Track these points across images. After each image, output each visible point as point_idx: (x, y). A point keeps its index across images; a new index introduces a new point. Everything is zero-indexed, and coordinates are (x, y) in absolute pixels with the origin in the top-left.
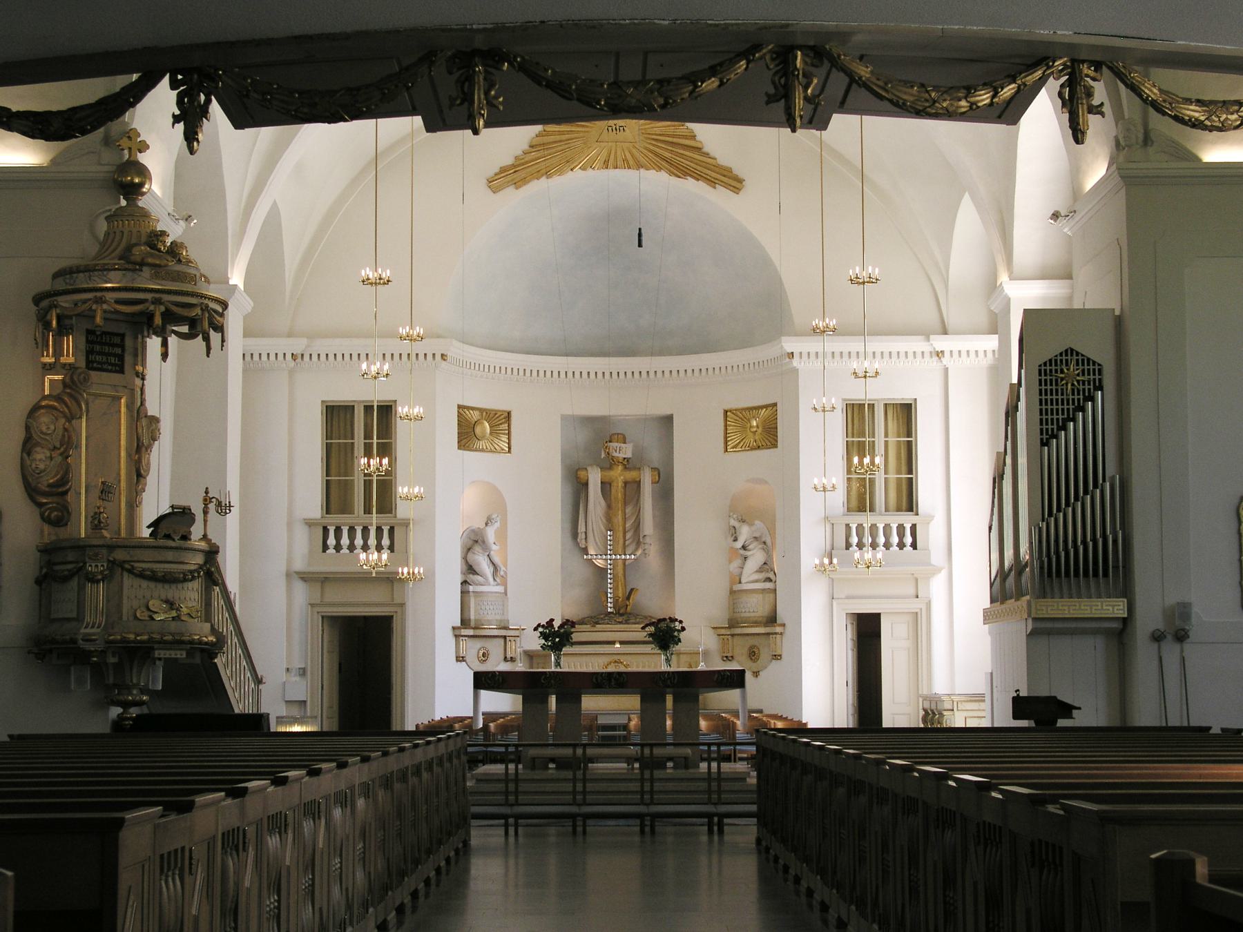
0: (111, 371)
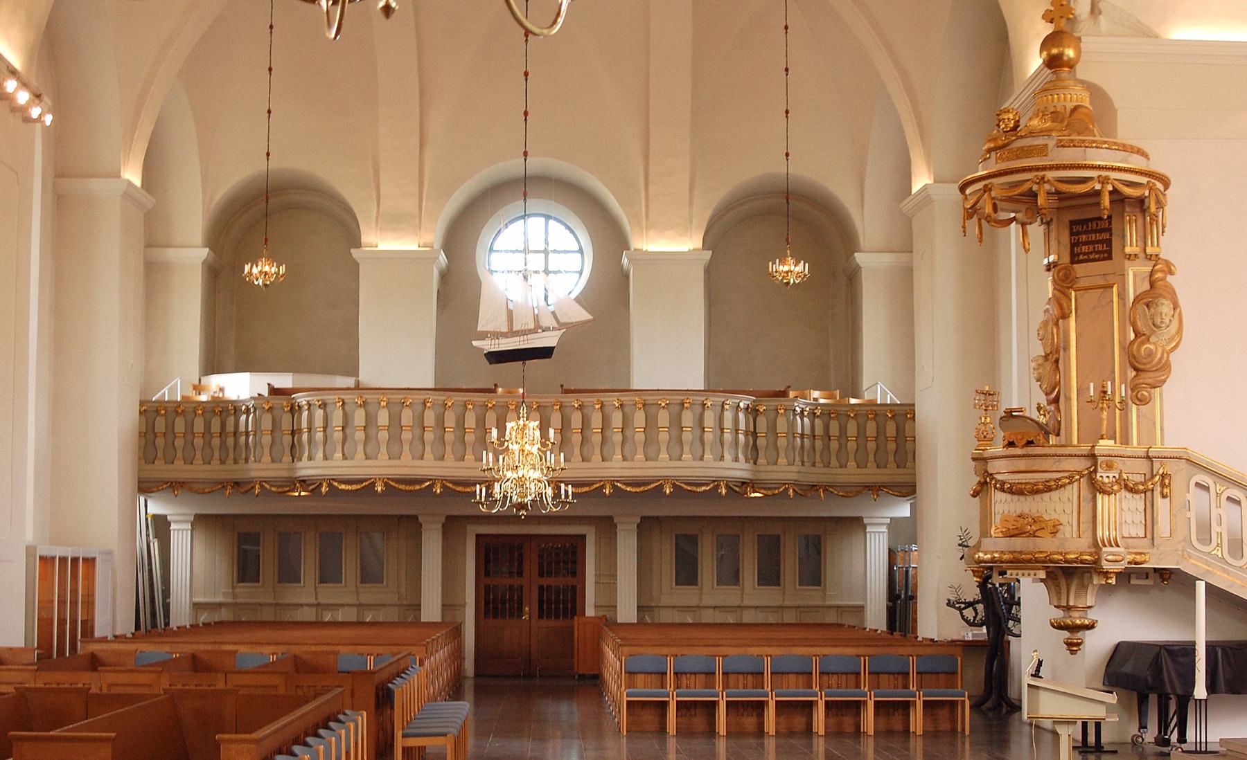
0: (1099, 260)
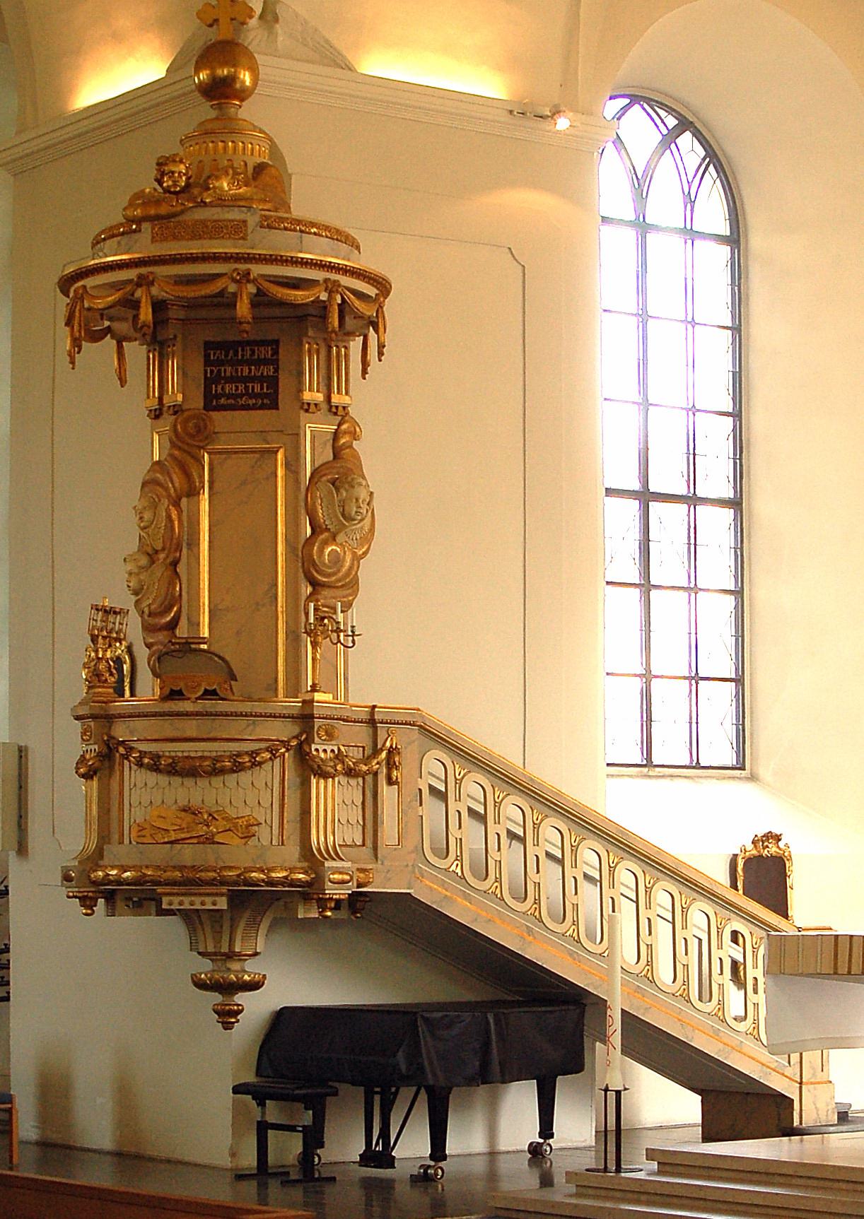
0: (253, 408)
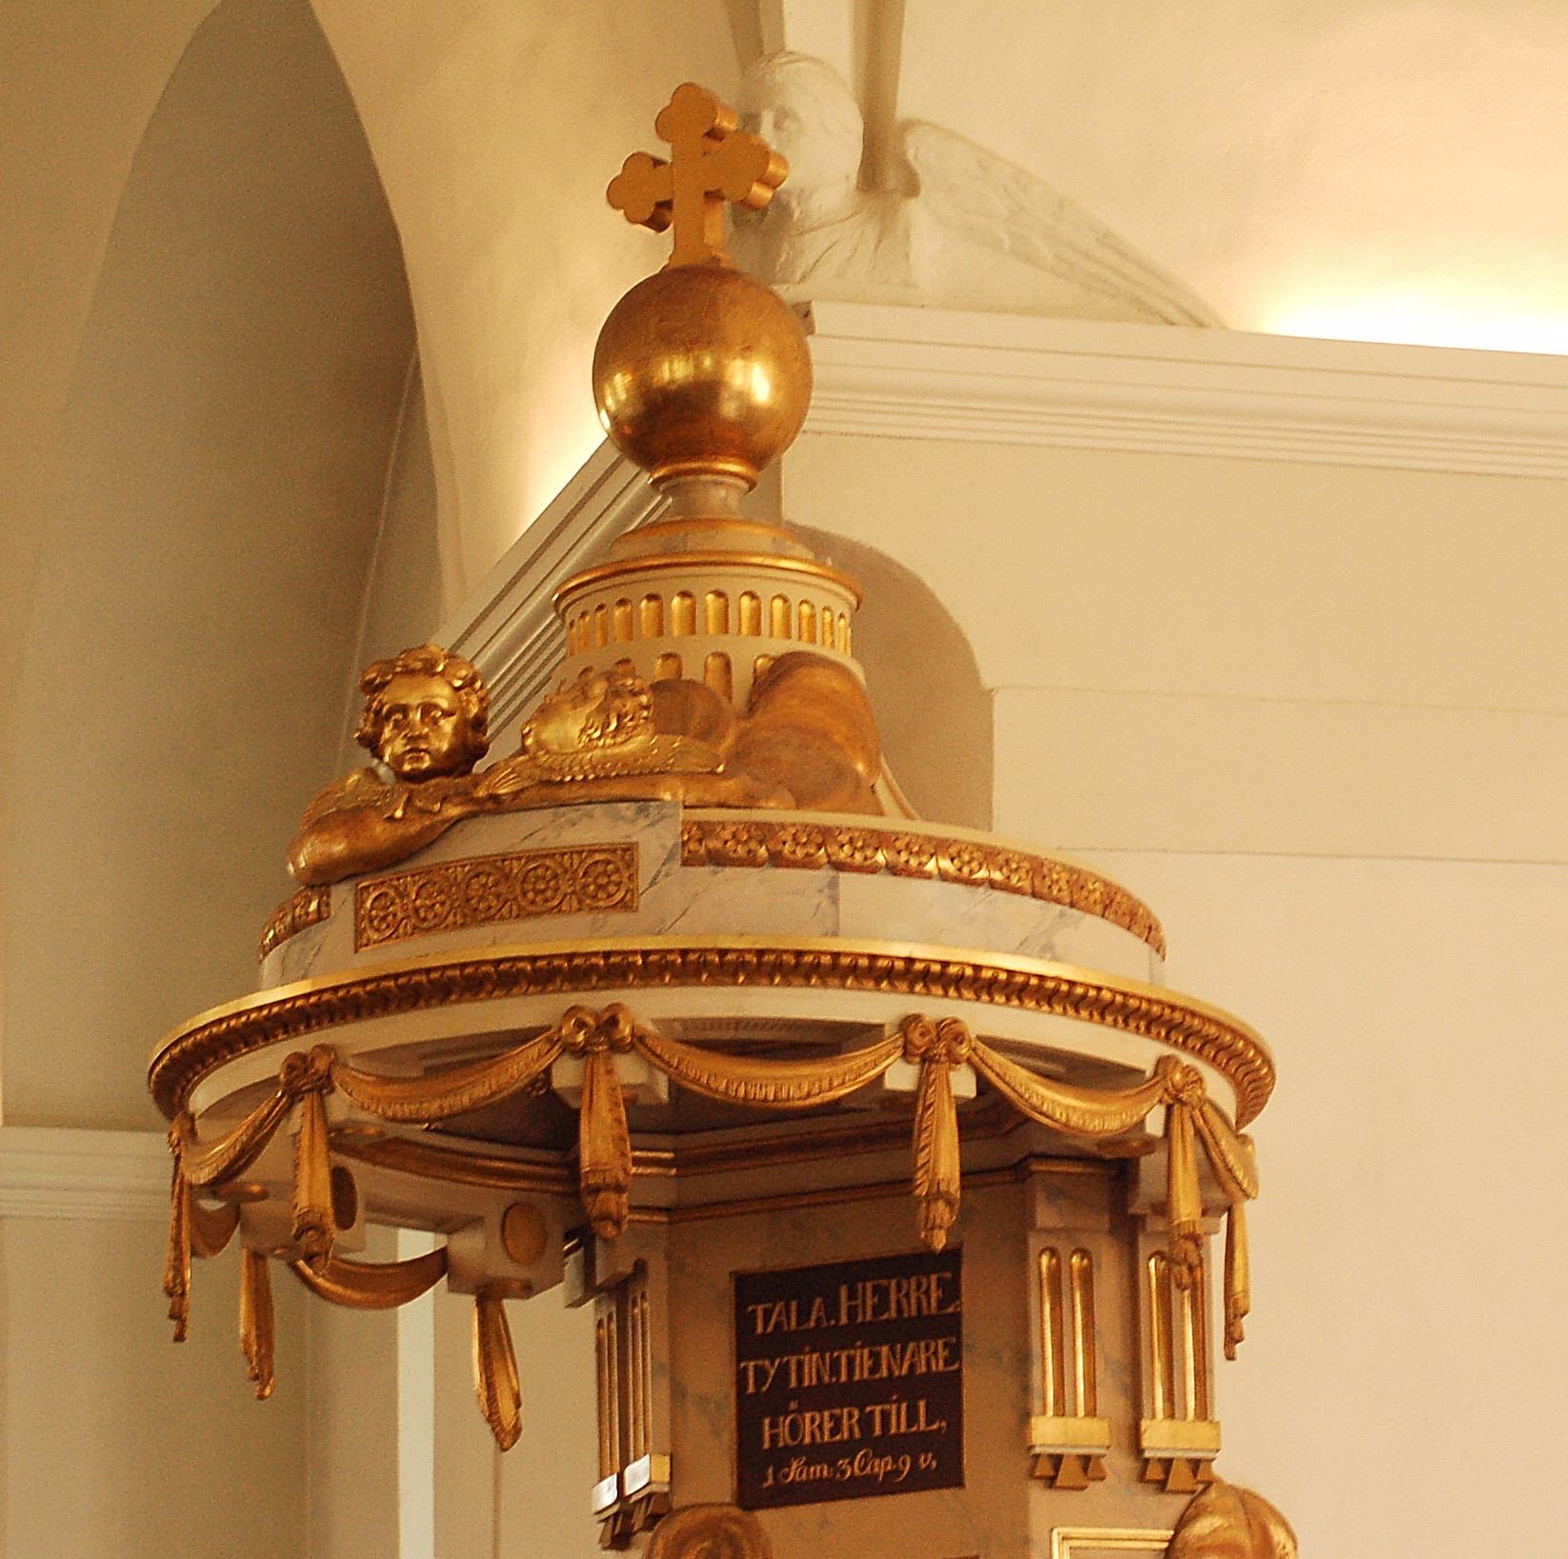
0: (888, 1486)
